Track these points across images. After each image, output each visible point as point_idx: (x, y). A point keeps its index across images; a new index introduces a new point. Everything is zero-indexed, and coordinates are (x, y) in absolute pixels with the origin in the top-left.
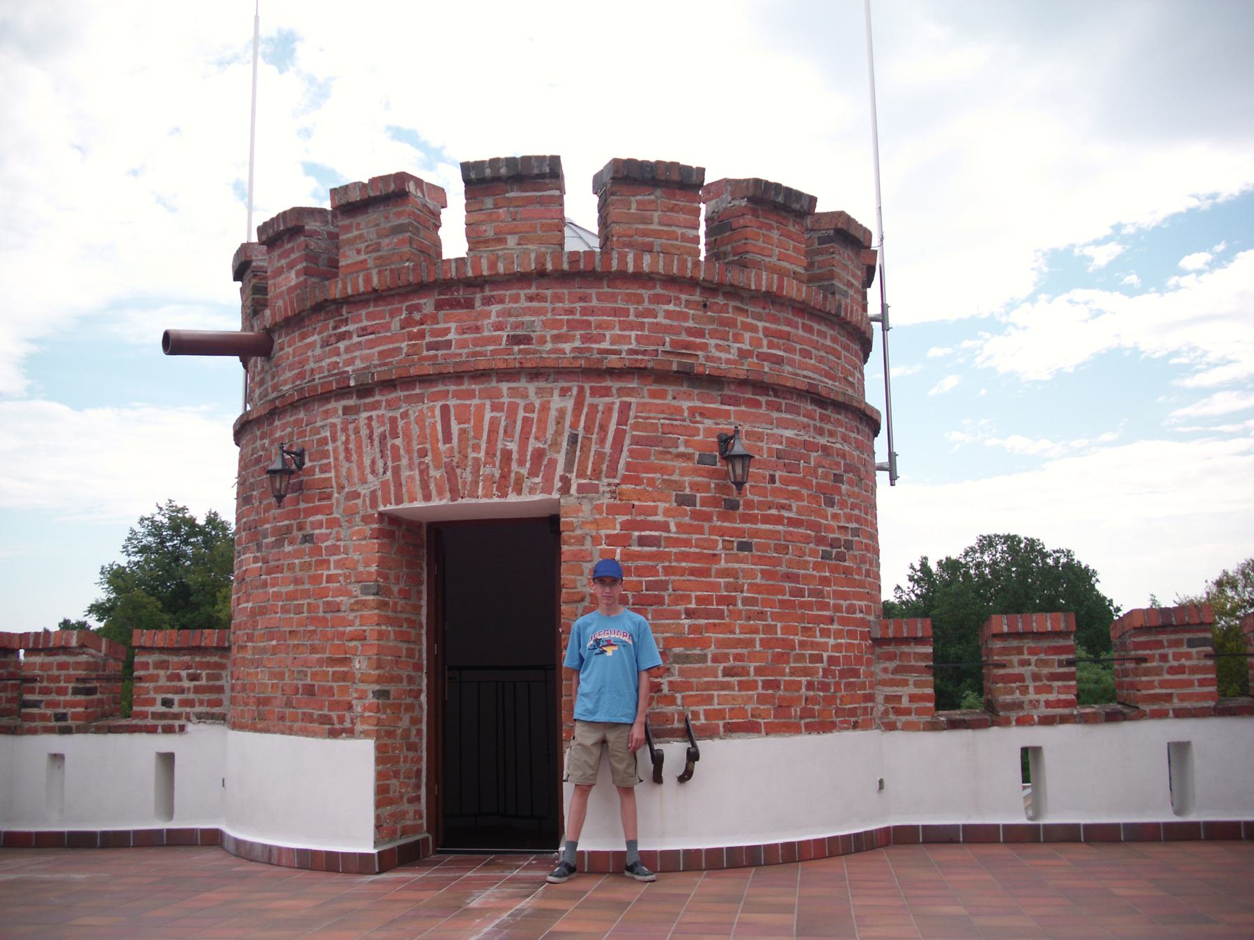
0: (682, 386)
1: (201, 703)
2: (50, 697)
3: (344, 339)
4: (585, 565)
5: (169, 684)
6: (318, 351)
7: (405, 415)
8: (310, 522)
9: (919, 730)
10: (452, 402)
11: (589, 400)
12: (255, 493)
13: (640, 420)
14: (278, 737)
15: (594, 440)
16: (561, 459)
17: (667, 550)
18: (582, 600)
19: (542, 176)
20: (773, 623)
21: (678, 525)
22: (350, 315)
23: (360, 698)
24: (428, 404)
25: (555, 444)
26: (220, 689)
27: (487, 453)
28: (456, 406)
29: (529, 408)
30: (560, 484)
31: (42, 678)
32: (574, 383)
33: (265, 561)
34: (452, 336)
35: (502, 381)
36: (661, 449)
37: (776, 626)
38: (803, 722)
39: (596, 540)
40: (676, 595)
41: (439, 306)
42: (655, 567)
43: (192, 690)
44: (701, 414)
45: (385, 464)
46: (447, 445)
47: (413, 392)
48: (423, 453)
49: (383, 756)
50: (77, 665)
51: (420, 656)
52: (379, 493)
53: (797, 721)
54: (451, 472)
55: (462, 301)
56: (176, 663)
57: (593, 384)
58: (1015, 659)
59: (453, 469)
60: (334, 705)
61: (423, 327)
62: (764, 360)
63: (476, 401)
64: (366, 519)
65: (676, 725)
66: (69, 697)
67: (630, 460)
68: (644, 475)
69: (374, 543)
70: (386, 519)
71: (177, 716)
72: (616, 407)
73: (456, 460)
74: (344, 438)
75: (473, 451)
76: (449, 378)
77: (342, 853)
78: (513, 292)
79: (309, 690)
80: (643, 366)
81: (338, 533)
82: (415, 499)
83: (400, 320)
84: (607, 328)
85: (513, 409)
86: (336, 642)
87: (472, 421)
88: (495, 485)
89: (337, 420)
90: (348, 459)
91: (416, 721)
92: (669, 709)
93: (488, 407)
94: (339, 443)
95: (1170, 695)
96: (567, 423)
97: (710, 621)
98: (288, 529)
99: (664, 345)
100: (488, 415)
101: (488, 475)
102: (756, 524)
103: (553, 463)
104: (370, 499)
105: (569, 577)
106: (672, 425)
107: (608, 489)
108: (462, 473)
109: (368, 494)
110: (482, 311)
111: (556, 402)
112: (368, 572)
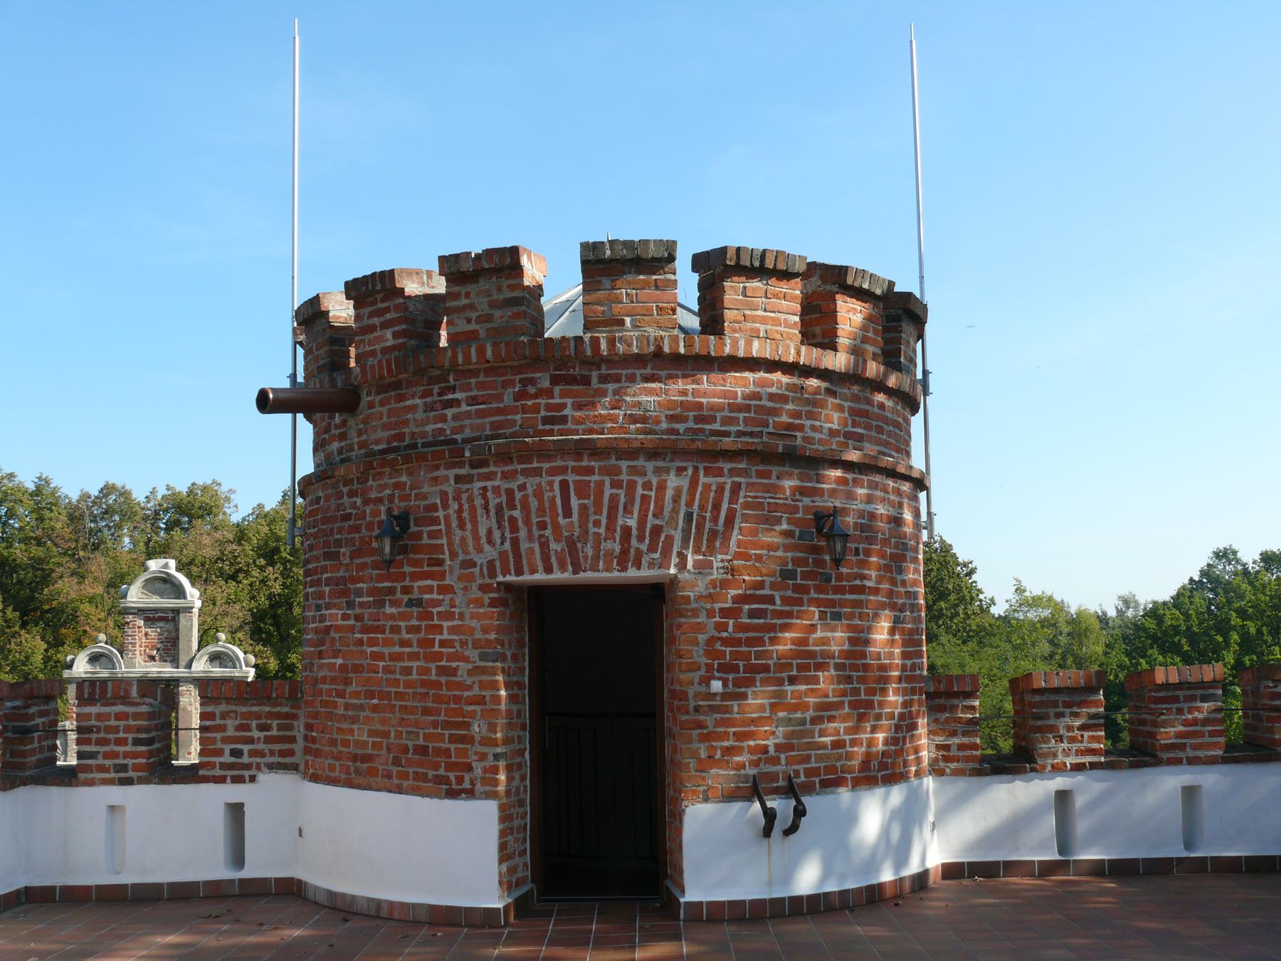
0: (784, 466)
1: (272, 753)
2: (107, 749)
3: (451, 407)
4: (700, 636)
5: (238, 734)
6: (420, 415)
7: (522, 487)
8: (419, 587)
9: (965, 775)
10: (571, 478)
11: (703, 480)
12: (342, 550)
13: (750, 499)
14: (384, 796)
15: (708, 518)
16: (678, 536)
17: (773, 621)
18: (699, 669)
19: (659, 260)
20: (858, 686)
21: (782, 598)
22: (458, 383)
23: (480, 760)
24: (545, 479)
25: (673, 521)
26: (292, 740)
27: (607, 528)
28: (575, 482)
29: (648, 486)
30: (677, 560)
31: (99, 728)
32: (689, 463)
33: (358, 618)
34: (568, 411)
35: (621, 459)
36: (767, 526)
37: (860, 688)
38: (880, 775)
39: (711, 614)
40: (780, 663)
41: (555, 380)
42: (763, 637)
43: (262, 740)
44: (802, 494)
45: (503, 535)
46: (568, 520)
47: (530, 466)
48: (542, 526)
49: (505, 817)
50: (137, 716)
51: (525, 716)
52: (498, 563)
53: (875, 774)
54: (571, 543)
55: (579, 377)
56: (245, 713)
57: (706, 464)
58: (1052, 711)
59: (574, 543)
60: (450, 767)
61: (537, 401)
62: (849, 439)
63: (596, 478)
64: (484, 588)
65: (781, 783)
66: (128, 748)
67: (741, 537)
68: (753, 552)
69: (493, 612)
70: (502, 587)
71: (248, 767)
72: (728, 487)
73: (576, 534)
74: (456, 507)
75: (594, 526)
76: (568, 454)
77: (465, 908)
78: (630, 371)
79: (422, 750)
80: (753, 448)
81: (452, 599)
82: (537, 571)
83: (514, 392)
84: (718, 410)
85: (632, 486)
86: (452, 706)
87: (592, 497)
88: (615, 560)
89: (449, 488)
90: (462, 526)
91: (523, 778)
92: (777, 768)
93: (607, 484)
94: (451, 511)
95: (1185, 744)
96: (683, 502)
97: (809, 687)
98: (391, 591)
99: (768, 426)
100: (608, 492)
101: (609, 550)
102: (845, 594)
103: (670, 539)
104: (488, 568)
105: (686, 647)
106: (776, 503)
107: (722, 565)
108: (583, 547)
109: (485, 564)
110: (599, 389)
111: (673, 481)
112: (486, 639)
